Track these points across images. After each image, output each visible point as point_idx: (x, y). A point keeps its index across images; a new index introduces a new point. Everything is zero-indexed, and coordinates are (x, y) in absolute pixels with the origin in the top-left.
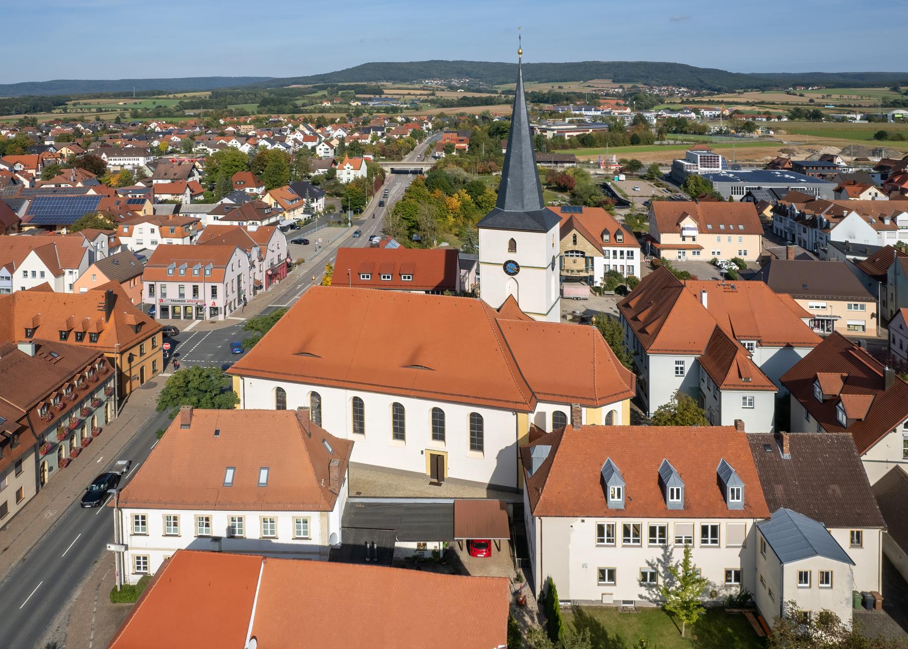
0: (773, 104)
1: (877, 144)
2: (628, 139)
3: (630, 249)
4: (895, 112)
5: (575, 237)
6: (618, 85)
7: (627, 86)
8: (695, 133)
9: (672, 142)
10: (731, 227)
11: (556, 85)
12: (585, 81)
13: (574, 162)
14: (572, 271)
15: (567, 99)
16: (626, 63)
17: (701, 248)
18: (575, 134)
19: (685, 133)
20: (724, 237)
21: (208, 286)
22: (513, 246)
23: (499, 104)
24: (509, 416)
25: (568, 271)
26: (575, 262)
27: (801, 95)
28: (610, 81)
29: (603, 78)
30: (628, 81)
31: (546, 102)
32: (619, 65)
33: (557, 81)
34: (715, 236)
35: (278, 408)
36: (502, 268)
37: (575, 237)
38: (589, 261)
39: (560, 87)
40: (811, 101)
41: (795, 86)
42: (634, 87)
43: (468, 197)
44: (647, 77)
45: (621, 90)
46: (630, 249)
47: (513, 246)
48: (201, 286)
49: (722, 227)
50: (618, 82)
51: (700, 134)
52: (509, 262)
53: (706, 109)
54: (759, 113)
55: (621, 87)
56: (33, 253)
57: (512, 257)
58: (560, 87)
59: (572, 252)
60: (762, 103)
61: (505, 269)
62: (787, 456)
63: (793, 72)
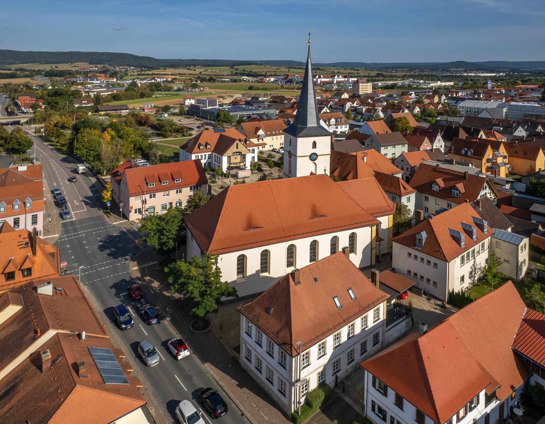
0: (185, 74)
1: (249, 91)
2: (139, 95)
3: (253, 148)
4: (243, 77)
5: (237, 144)
6: (94, 66)
7: (100, 66)
8: (165, 90)
9: (158, 96)
10: (269, 133)
11: (54, 66)
12: (72, 63)
13: (127, 109)
14: (237, 163)
15: (70, 74)
16: (97, 53)
17: (265, 144)
18: (106, 94)
19: (160, 90)
20: (275, 137)
21: (29, 216)
22: (314, 145)
23: (20, 77)
24: (368, 229)
25: (234, 164)
26: (236, 158)
27: (194, 70)
28: (87, 63)
29: (83, 61)
30: (99, 63)
31: (55, 76)
32: (93, 54)
33: (55, 63)
34: (271, 137)
35: (332, 253)
36: (308, 158)
37: (237, 144)
38: (244, 157)
39: (56, 67)
40: (200, 73)
41: (190, 65)
42: (104, 67)
43: (113, 133)
44: (110, 61)
45: (96, 69)
46: (253, 148)
47: (314, 145)
48: (22, 217)
49: (274, 132)
50: (93, 64)
51: (169, 91)
52: (313, 154)
53: (159, 78)
54: (186, 79)
55: (96, 67)
56: (298, 175)
57: (314, 151)
58: (56, 67)
59: (237, 152)
60: (180, 74)
61: (310, 158)
62: (481, 209)
63: (183, 59)
